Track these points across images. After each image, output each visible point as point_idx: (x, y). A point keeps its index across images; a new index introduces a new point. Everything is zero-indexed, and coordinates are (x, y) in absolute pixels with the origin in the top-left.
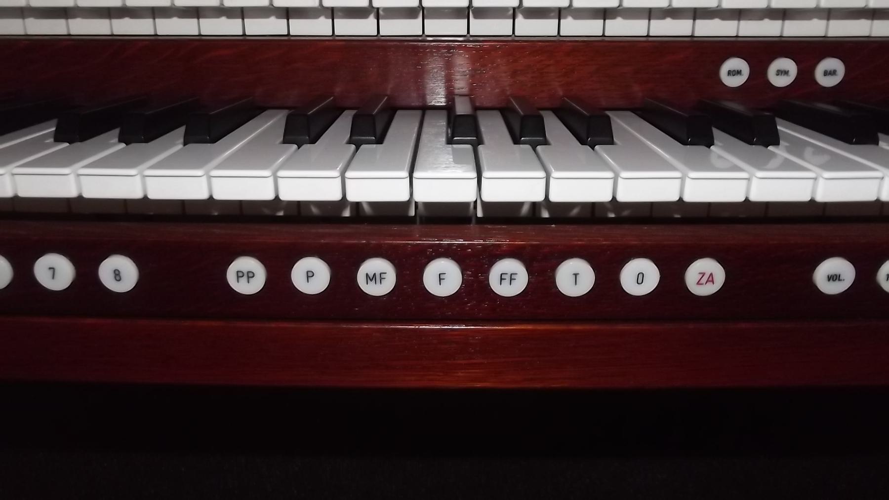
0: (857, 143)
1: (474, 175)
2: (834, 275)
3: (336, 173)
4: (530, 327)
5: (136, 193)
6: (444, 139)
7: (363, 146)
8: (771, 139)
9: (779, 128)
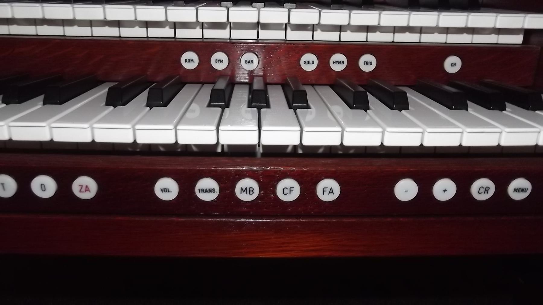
0: (455, 109)
2: (406, 190)
3: (171, 127)
4: (354, 220)
5: (45, 137)
6: (246, 105)
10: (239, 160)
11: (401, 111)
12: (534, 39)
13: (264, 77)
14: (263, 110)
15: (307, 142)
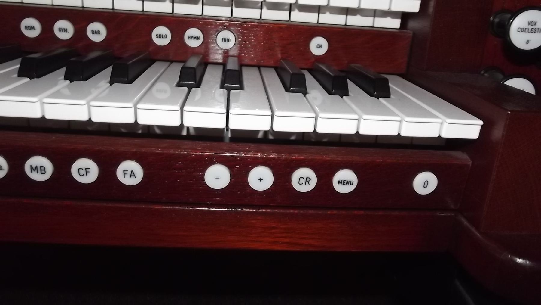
1: (269, 113)
2: (217, 177)
6: (218, 85)
8: (343, 92)
9: (390, 85)
10: (208, 144)
11: (378, 99)
12: (412, 24)
13: (239, 57)
14: (232, 91)
15: (277, 128)
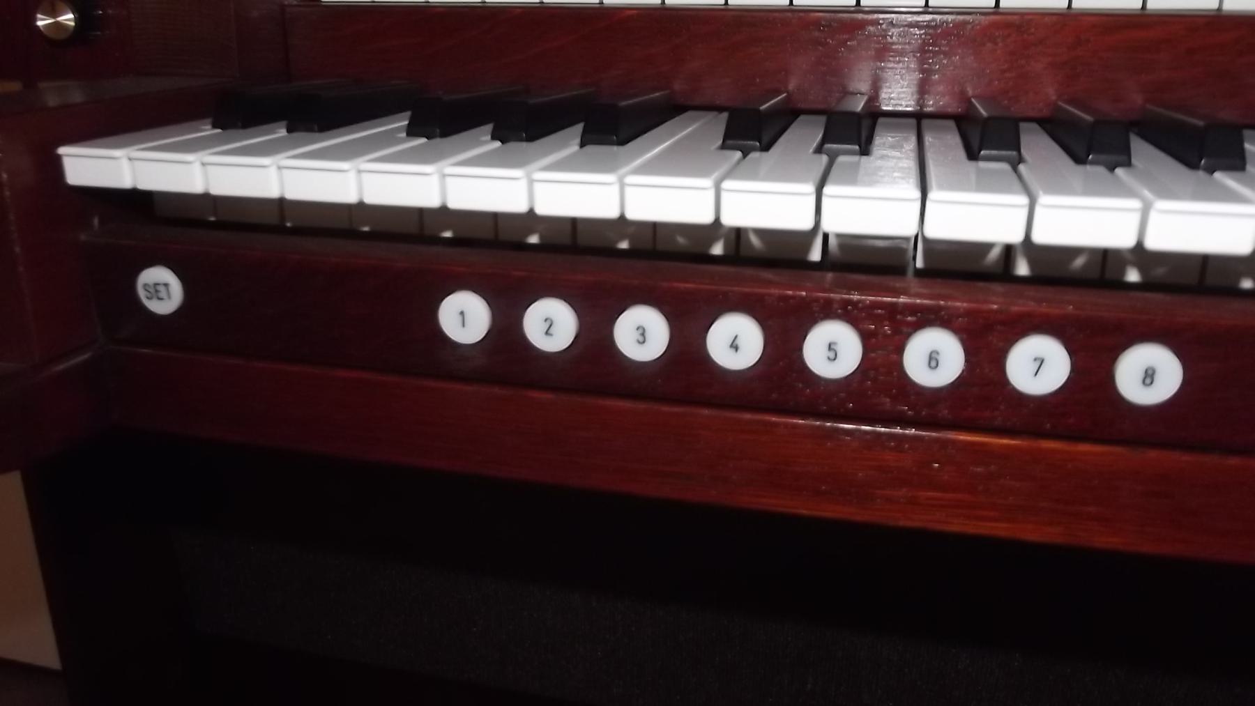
2: (464, 317)
7: (841, 159)
9: (1247, 146)
